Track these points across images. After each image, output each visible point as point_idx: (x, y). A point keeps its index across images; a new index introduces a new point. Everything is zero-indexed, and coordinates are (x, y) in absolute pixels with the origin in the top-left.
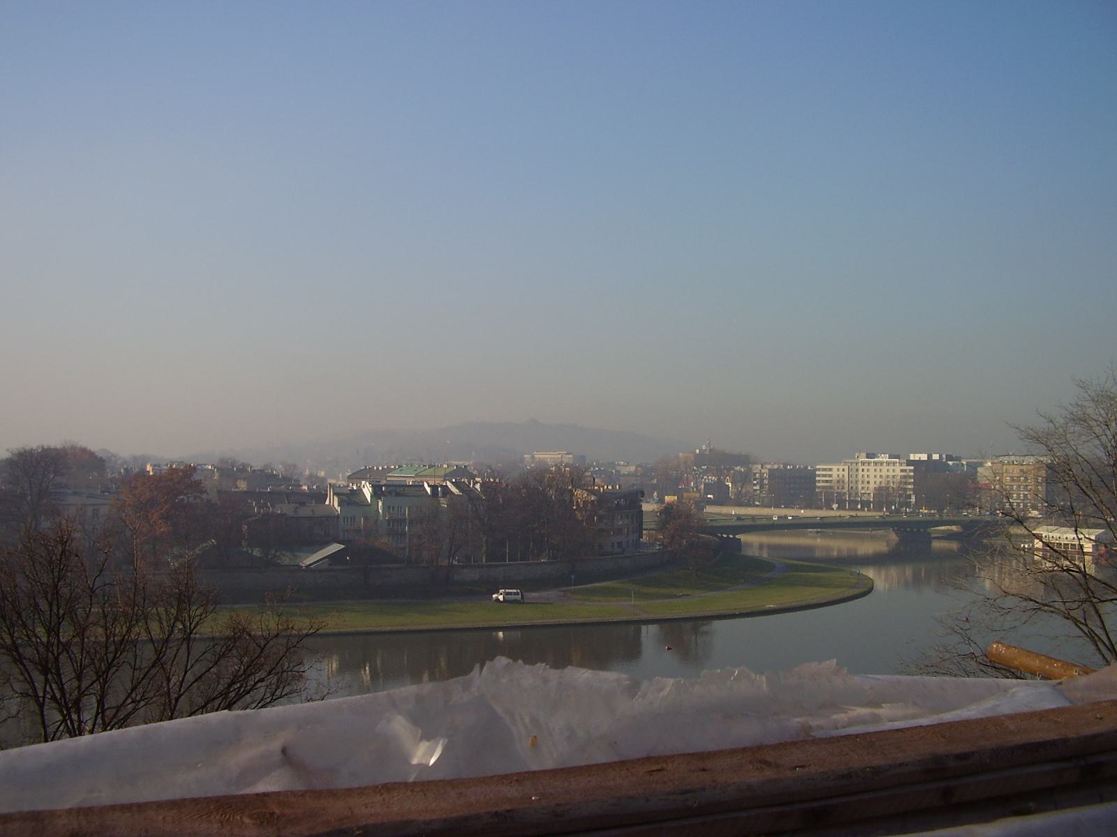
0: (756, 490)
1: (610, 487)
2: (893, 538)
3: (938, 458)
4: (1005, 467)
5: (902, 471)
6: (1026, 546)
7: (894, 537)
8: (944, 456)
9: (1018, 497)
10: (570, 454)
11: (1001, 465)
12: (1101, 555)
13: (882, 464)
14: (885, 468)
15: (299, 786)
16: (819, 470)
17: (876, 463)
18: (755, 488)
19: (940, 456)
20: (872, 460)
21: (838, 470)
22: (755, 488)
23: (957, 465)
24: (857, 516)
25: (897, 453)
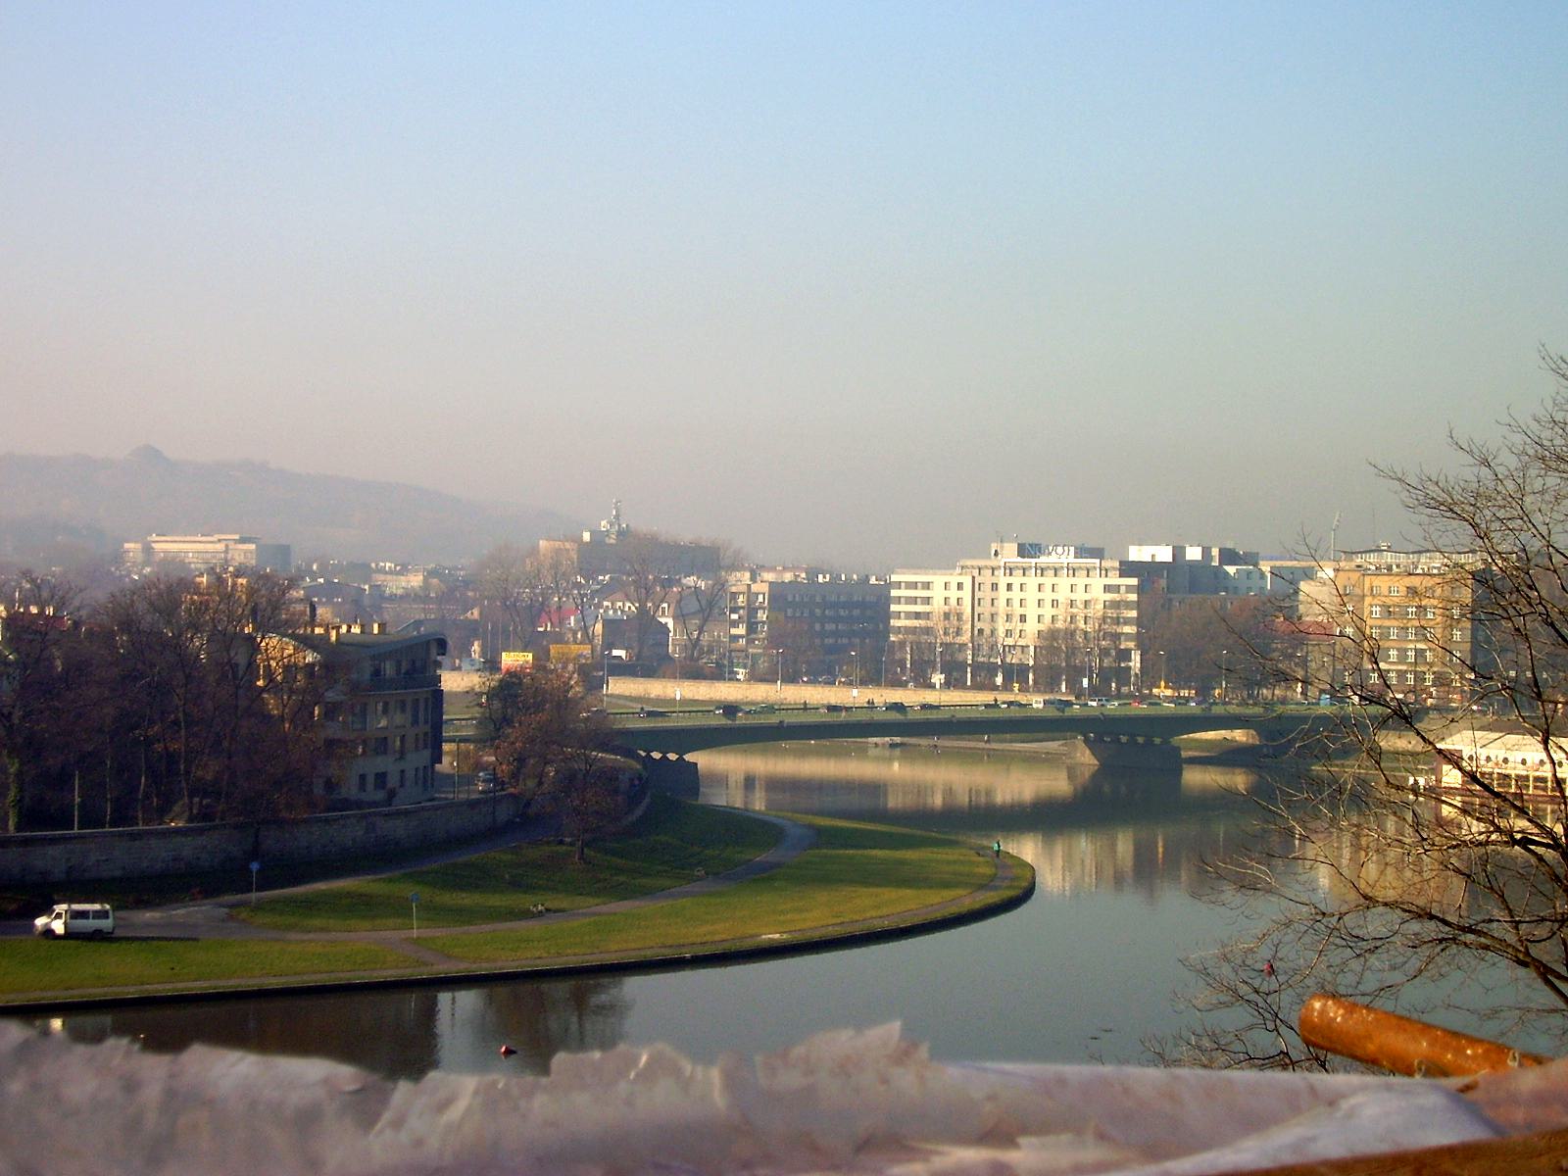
1: (356, 630)
3: (1199, 557)
5: (1107, 588)
6: (1422, 781)
7: (1085, 758)
8: (1215, 552)
14: (1064, 582)
16: (898, 585)
18: (734, 631)
19: (1206, 552)
22: (734, 631)
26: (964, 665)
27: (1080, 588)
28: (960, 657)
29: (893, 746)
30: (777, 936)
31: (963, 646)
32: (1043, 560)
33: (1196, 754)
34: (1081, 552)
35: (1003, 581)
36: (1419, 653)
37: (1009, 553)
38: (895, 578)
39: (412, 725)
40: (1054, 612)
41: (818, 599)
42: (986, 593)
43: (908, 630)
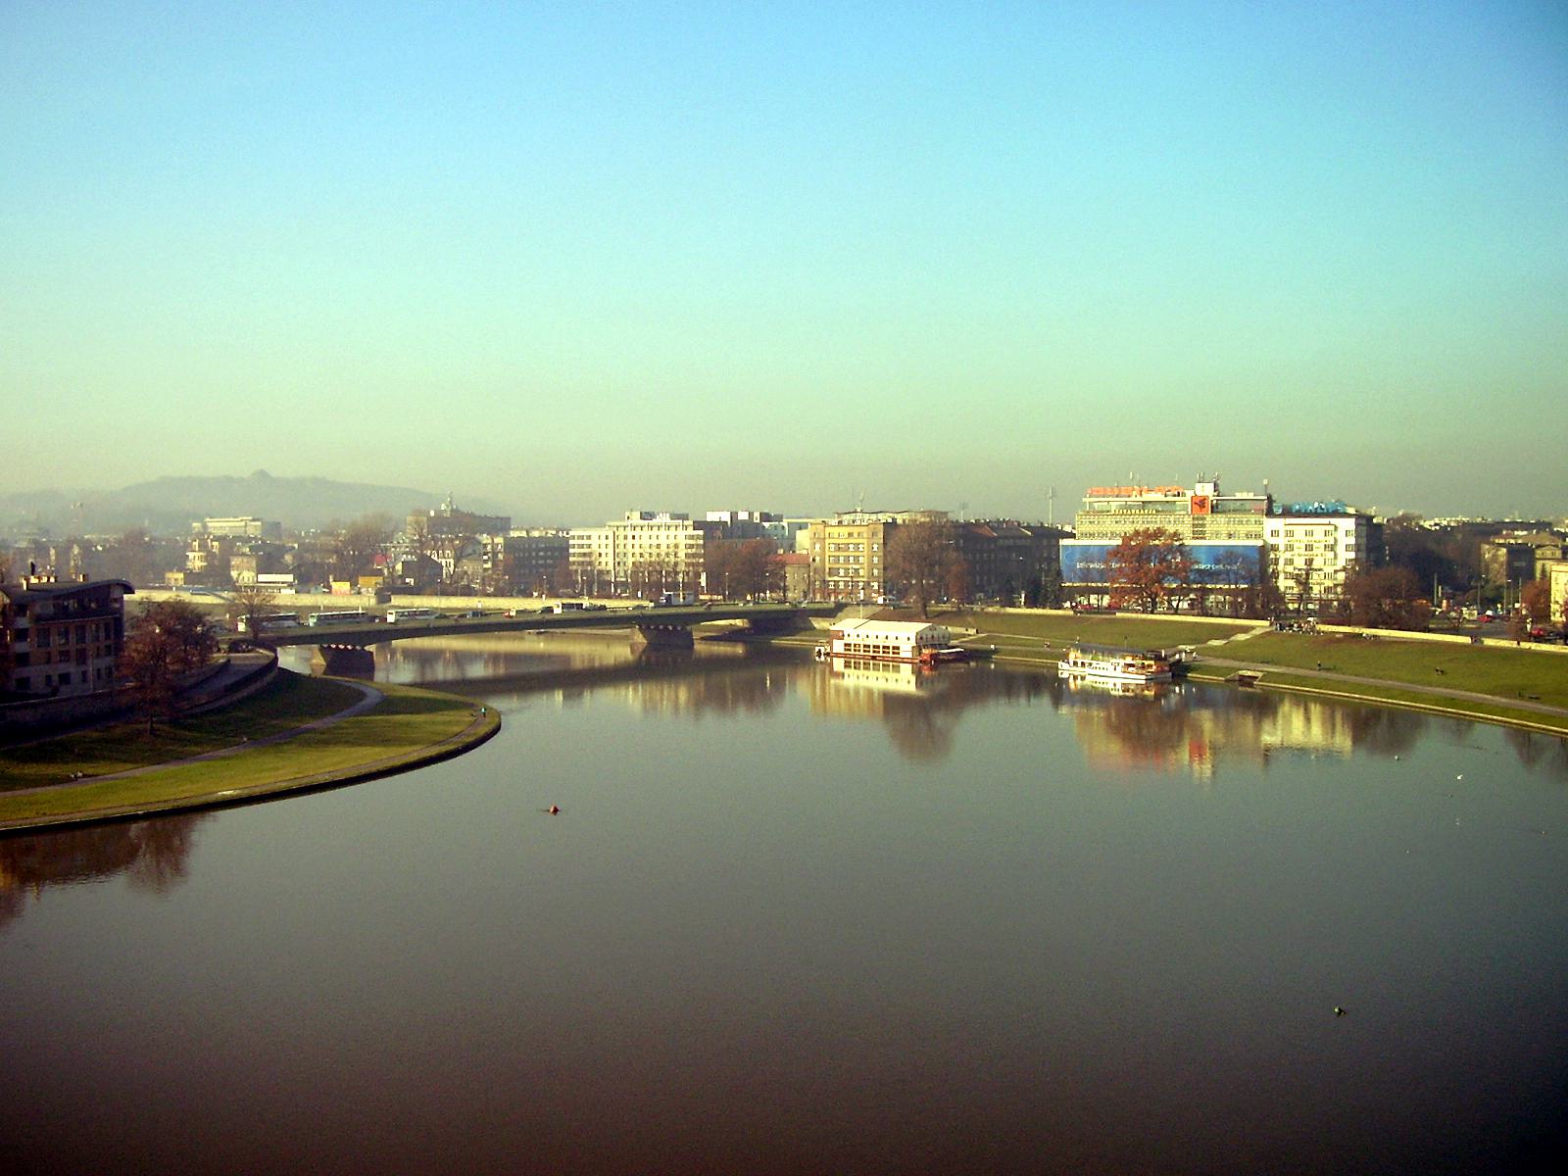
0: (488, 569)
1: (52, 580)
2: (640, 641)
3: (747, 518)
4: (828, 530)
7: (640, 639)
8: (757, 515)
10: (258, 520)
11: (822, 526)
14: (663, 533)
16: (573, 538)
18: (486, 566)
19: (751, 515)
22: (486, 566)
24: (604, 608)
27: (672, 537)
28: (607, 578)
31: (608, 572)
32: (651, 523)
33: (713, 634)
34: (674, 517)
35: (630, 533)
36: (857, 570)
37: (636, 518)
38: (571, 533)
39: (106, 639)
40: (658, 551)
41: (534, 546)
42: (621, 541)
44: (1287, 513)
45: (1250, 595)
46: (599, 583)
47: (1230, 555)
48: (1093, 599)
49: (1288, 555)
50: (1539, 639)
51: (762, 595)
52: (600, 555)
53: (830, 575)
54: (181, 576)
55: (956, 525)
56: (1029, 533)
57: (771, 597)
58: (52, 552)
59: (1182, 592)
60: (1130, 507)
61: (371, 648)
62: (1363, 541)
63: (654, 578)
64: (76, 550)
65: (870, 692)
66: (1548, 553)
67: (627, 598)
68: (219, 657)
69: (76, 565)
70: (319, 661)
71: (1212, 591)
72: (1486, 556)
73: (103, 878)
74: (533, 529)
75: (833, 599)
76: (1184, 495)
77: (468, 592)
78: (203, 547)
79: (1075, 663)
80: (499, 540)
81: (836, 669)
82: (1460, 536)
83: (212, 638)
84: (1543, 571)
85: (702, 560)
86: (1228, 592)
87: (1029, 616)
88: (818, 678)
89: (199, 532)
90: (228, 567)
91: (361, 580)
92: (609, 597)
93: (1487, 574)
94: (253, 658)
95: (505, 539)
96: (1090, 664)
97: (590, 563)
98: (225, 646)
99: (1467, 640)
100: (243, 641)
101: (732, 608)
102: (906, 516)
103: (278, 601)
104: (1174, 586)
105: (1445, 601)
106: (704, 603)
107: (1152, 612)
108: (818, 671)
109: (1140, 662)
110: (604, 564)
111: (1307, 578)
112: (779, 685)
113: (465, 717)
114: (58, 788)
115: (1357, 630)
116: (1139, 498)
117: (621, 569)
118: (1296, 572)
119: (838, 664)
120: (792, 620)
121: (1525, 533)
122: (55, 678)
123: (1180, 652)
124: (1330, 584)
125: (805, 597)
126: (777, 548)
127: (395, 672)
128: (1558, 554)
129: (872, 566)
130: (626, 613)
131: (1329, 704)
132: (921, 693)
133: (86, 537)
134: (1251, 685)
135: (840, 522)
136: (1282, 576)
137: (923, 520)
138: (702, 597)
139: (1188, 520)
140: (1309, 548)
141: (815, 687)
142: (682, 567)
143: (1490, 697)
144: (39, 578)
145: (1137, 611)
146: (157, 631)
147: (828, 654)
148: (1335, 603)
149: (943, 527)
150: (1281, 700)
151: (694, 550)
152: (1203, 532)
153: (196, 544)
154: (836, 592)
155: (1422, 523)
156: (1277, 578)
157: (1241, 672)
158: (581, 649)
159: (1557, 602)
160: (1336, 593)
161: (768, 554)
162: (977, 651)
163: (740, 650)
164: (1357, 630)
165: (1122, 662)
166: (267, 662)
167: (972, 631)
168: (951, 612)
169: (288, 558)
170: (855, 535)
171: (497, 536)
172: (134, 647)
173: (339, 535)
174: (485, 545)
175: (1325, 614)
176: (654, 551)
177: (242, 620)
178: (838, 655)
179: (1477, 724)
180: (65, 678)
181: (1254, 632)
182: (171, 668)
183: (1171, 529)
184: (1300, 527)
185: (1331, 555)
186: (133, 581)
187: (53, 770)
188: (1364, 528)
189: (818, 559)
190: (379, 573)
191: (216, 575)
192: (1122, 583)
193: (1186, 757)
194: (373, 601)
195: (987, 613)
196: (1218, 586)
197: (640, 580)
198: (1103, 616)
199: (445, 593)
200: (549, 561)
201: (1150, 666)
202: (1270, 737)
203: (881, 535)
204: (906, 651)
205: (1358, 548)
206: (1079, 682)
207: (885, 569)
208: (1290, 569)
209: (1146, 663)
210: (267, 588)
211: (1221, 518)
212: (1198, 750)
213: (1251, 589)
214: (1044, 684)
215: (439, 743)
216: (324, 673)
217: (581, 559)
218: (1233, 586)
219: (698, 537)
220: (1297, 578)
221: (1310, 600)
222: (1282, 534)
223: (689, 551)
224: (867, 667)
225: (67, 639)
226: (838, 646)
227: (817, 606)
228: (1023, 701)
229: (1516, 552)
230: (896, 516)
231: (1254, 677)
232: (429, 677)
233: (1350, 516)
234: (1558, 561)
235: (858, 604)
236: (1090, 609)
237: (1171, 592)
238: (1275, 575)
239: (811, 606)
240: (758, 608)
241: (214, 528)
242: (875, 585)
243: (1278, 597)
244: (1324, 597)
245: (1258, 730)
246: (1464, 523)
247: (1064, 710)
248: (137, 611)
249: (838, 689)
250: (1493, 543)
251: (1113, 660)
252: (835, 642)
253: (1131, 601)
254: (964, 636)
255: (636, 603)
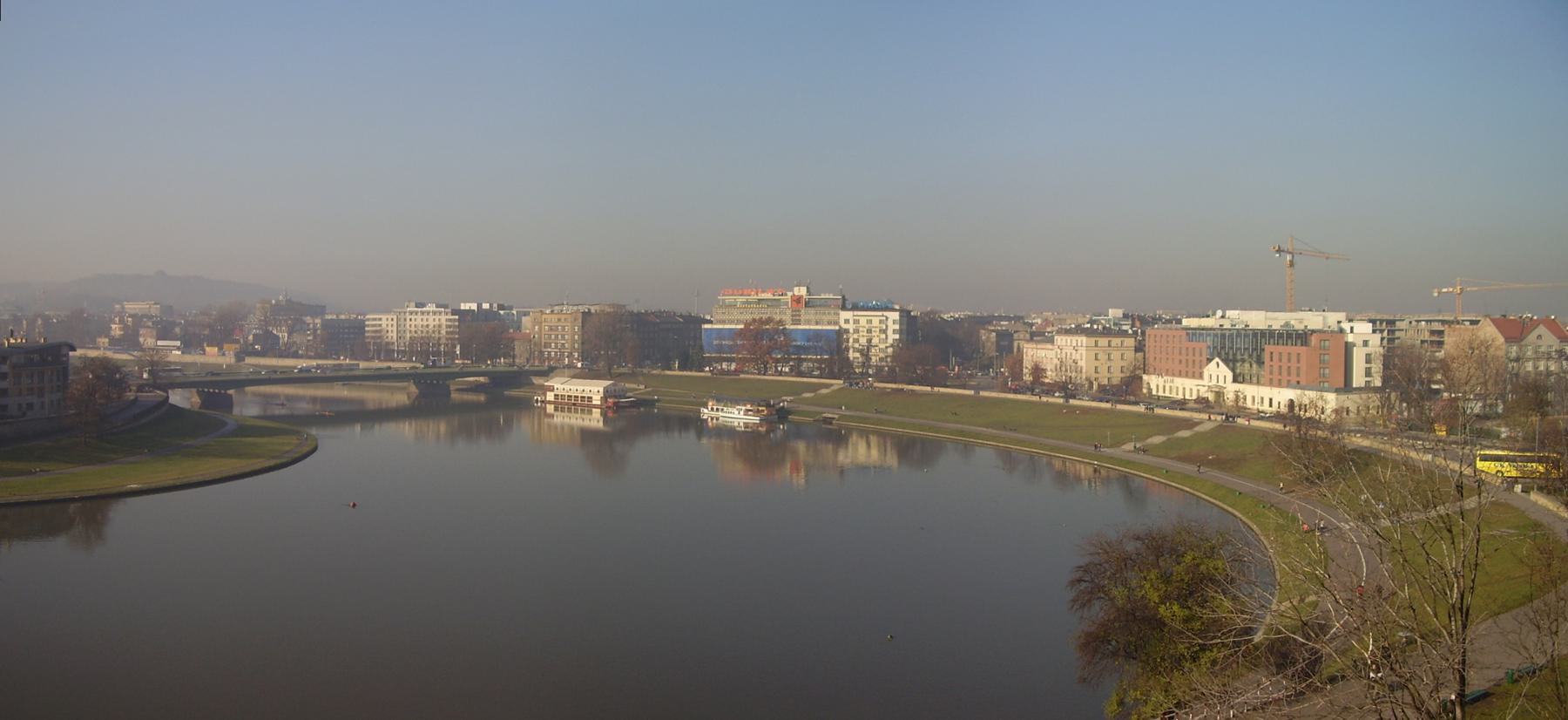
1: (24, 341)
4: (544, 316)
5: (447, 320)
6: (539, 398)
7: (413, 389)
8: (495, 305)
9: (556, 347)
10: (158, 304)
12: (608, 407)
13: (428, 313)
14: (431, 317)
15: (1325, 394)
16: (368, 320)
17: (423, 313)
19: (491, 306)
20: (420, 309)
21: (387, 319)
22: (309, 338)
23: (508, 314)
24: (390, 368)
25: (446, 303)
26: (394, 350)
28: (392, 347)
29: (344, 384)
30: (135, 486)
31: (393, 343)
36: (563, 344)
38: (367, 317)
42: (402, 322)
43: (373, 338)
44: (855, 308)
45: (830, 363)
46: (385, 351)
47: (817, 335)
48: (724, 366)
49: (856, 336)
50: (1016, 391)
51: (498, 360)
52: (388, 331)
53: (545, 347)
54: (107, 340)
55: (631, 314)
56: (681, 320)
57: (505, 363)
58: (25, 322)
59: (785, 361)
60: (750, 303)
61: (231, 392)
62: (904, 327)
63: (424, 348)
64: (40, 322)
65: (571, 428)
66: (1022, 336)
67: (406, 361)
68: (131, 395)
69: (39, 333)
70: (196, 399)
71: (805, 360)
72: (983, 338)
73: (51, 538)
74: (341, 314)
75: (547, 364)
76: (786, 295)
77: (296, 356)
78: (121, 321)
79: (712, 409)
80: (318, 321)
81: (548, 411)
82: (966, 325)
83: (126, 383)
84: (1019, 347)
85: (457, 336)
86: (816, 361)
87: (681, 376)
88: (536, 418)
89: (119, 312)
90: (137, 335)
91: (226, 346)
92: (393, 360)
93: (983, 350)
94: (152, 396)
95: (322, 320)
96: (722, 410)
97: (380, 337)
98: (134, 388)
99: (972, 392)
100: (147, 385)
101: (477, 369)
102: (597, 308)
103: (170, 359)
104: (779, 356)
105: (957, 368)
106: (458, 365)
107: (764, 375)
108: (536, 414)
109: (756, 408)
110: (390, 338)
111: (868, 352)
112: (509, 422)
113: (293, 440)
114: (24, 478)
115: (900, 386)
116: (755, 297)
117: (401, 341)
118: (861, 347)
119: (550, 409)
120: (519, 378)
121: (1006, 323)
122: (24, 406)
123: (783, 401)
124: (882, 355)
125: (528, 362)
126: (509, 328)
127: (247, 408)
128: (1028, 336)
129: (574, 341)
130: (405, 371)
131: (882, 435)
132: (606, 429)
133: (47, 313)
134: (831, 424)
135: (552, 311)
136: (851, 351)
137: (609, 310)
138: (457, 362)
139: (789, 312)
140: (869, 331)
141: (533, 424)
142: (443, 341)
143: (985, 429)
144: (16, 340)
145: (754, 374)
146: (90, 376)
147: (542, 402)
148: (886, 368)
149: (623, 315)
150: (851, 433)
151: (452, 329)
152: (800, 320)
153: (117, 319)
154: (549, 358)
155: (942, 315)
156: (848, 351)
157: (824, 415)
158: (372, 396)
159: (1027, 368)
160: (887, 362)
161: (502, 332)
162: (645, 400)
163: (482, 398)
164: (900, 386)
165: (744, 408)
166: (160, 399)
167: (642, 387)
168: (628, 374)
169: (177, 330)
170: (563, 320)
171: (317, 318)
172: (75, 386)
173: (212, 315)
174: (309, 324)
175: (880, 375)
176: (425, 329)
177: (146, 371)
178: (550, 402)
179: (977, 448)
180: (30, 406)
181: (832, 388)
182: (99, 401)
183: (778, 318)
184: (863, 317)
185: (883, 336)
186: (75, 342)
187: (21, 466)
188: (905, 319)
189: (536, 336)
190: (237, 342)
191: (129, 340)
192: (744, 354)
193: (788, 472)
194: (233, 360)
195: (653, 375)
196: (809, 357)
197: (415, 349)
198: (732, 377)
199: (281, 356)
200: (352, 336)
201: (763, 411)
202: (844, 457)
203: (580, 320)
204: (597, 400)
205: (900, 332)
206: (715, 421)
207: (583, 343)
208: (857, 345)
209: (760, 408)
210: (162, 350)
211: (812, 311)
212: (796, 468)
213: (831, 359)
214: (696, 425)
215: (273, 457)
216: (200, 408)
217: (373, 335)
218: (819, 357)
219: (455, 320)
220: (861, 351)
221: (870, 366)
222: (851, 322)
223: (449, 330)
224: (569, 410)
225: (32, 381)
226: (550, 396)
227: (536, 369)
228: (676, 434)
229: (1001, 335)
230: (590, 307)
231: (834, 418)
232: (269, 412)
233: (896, 310)
234: (1028, 341)
235: (564, 368)
236: (722, 372)
237: (777, 361)
238: (847, 349)
239: (532, 369)
240: (495, 369)
241: (130, 309)
242: (576, 355)
243: (847, 363)
244: (879, 364)
245: (836, 453)
246: (969, 316)
247: (705, 441)
248: (78, 363)
249: (549, 426)
250: (988, 330)
251: (738, 407)
252: (548, 393)
253: (749, 367)
254: (636, 390)
255: (412, 365)
